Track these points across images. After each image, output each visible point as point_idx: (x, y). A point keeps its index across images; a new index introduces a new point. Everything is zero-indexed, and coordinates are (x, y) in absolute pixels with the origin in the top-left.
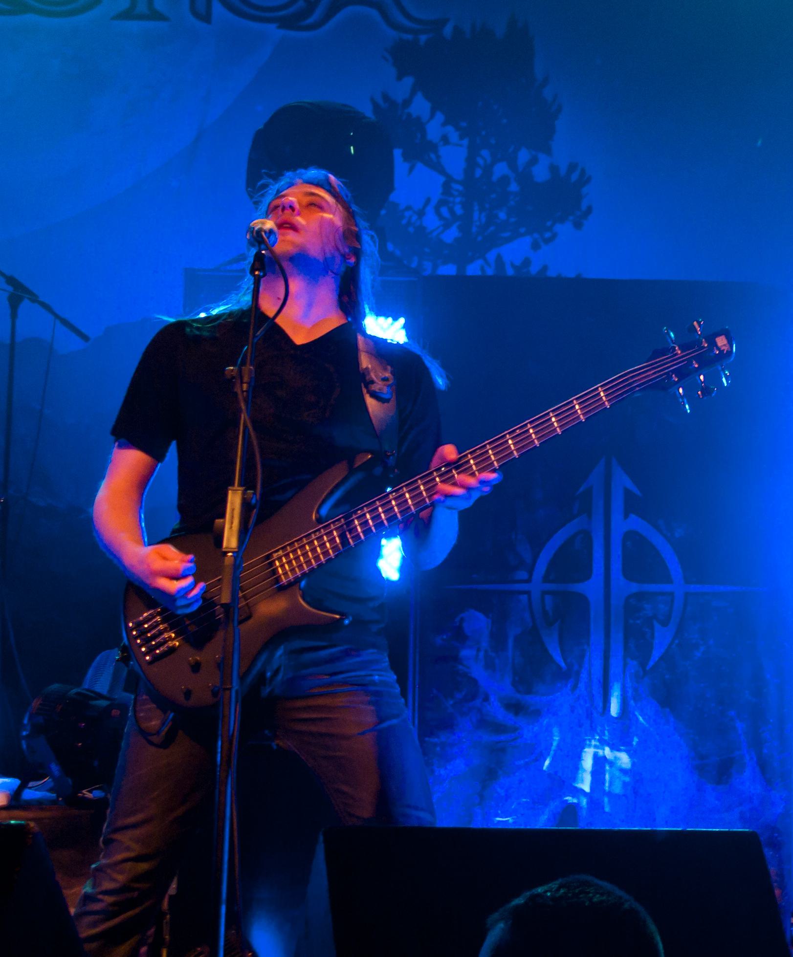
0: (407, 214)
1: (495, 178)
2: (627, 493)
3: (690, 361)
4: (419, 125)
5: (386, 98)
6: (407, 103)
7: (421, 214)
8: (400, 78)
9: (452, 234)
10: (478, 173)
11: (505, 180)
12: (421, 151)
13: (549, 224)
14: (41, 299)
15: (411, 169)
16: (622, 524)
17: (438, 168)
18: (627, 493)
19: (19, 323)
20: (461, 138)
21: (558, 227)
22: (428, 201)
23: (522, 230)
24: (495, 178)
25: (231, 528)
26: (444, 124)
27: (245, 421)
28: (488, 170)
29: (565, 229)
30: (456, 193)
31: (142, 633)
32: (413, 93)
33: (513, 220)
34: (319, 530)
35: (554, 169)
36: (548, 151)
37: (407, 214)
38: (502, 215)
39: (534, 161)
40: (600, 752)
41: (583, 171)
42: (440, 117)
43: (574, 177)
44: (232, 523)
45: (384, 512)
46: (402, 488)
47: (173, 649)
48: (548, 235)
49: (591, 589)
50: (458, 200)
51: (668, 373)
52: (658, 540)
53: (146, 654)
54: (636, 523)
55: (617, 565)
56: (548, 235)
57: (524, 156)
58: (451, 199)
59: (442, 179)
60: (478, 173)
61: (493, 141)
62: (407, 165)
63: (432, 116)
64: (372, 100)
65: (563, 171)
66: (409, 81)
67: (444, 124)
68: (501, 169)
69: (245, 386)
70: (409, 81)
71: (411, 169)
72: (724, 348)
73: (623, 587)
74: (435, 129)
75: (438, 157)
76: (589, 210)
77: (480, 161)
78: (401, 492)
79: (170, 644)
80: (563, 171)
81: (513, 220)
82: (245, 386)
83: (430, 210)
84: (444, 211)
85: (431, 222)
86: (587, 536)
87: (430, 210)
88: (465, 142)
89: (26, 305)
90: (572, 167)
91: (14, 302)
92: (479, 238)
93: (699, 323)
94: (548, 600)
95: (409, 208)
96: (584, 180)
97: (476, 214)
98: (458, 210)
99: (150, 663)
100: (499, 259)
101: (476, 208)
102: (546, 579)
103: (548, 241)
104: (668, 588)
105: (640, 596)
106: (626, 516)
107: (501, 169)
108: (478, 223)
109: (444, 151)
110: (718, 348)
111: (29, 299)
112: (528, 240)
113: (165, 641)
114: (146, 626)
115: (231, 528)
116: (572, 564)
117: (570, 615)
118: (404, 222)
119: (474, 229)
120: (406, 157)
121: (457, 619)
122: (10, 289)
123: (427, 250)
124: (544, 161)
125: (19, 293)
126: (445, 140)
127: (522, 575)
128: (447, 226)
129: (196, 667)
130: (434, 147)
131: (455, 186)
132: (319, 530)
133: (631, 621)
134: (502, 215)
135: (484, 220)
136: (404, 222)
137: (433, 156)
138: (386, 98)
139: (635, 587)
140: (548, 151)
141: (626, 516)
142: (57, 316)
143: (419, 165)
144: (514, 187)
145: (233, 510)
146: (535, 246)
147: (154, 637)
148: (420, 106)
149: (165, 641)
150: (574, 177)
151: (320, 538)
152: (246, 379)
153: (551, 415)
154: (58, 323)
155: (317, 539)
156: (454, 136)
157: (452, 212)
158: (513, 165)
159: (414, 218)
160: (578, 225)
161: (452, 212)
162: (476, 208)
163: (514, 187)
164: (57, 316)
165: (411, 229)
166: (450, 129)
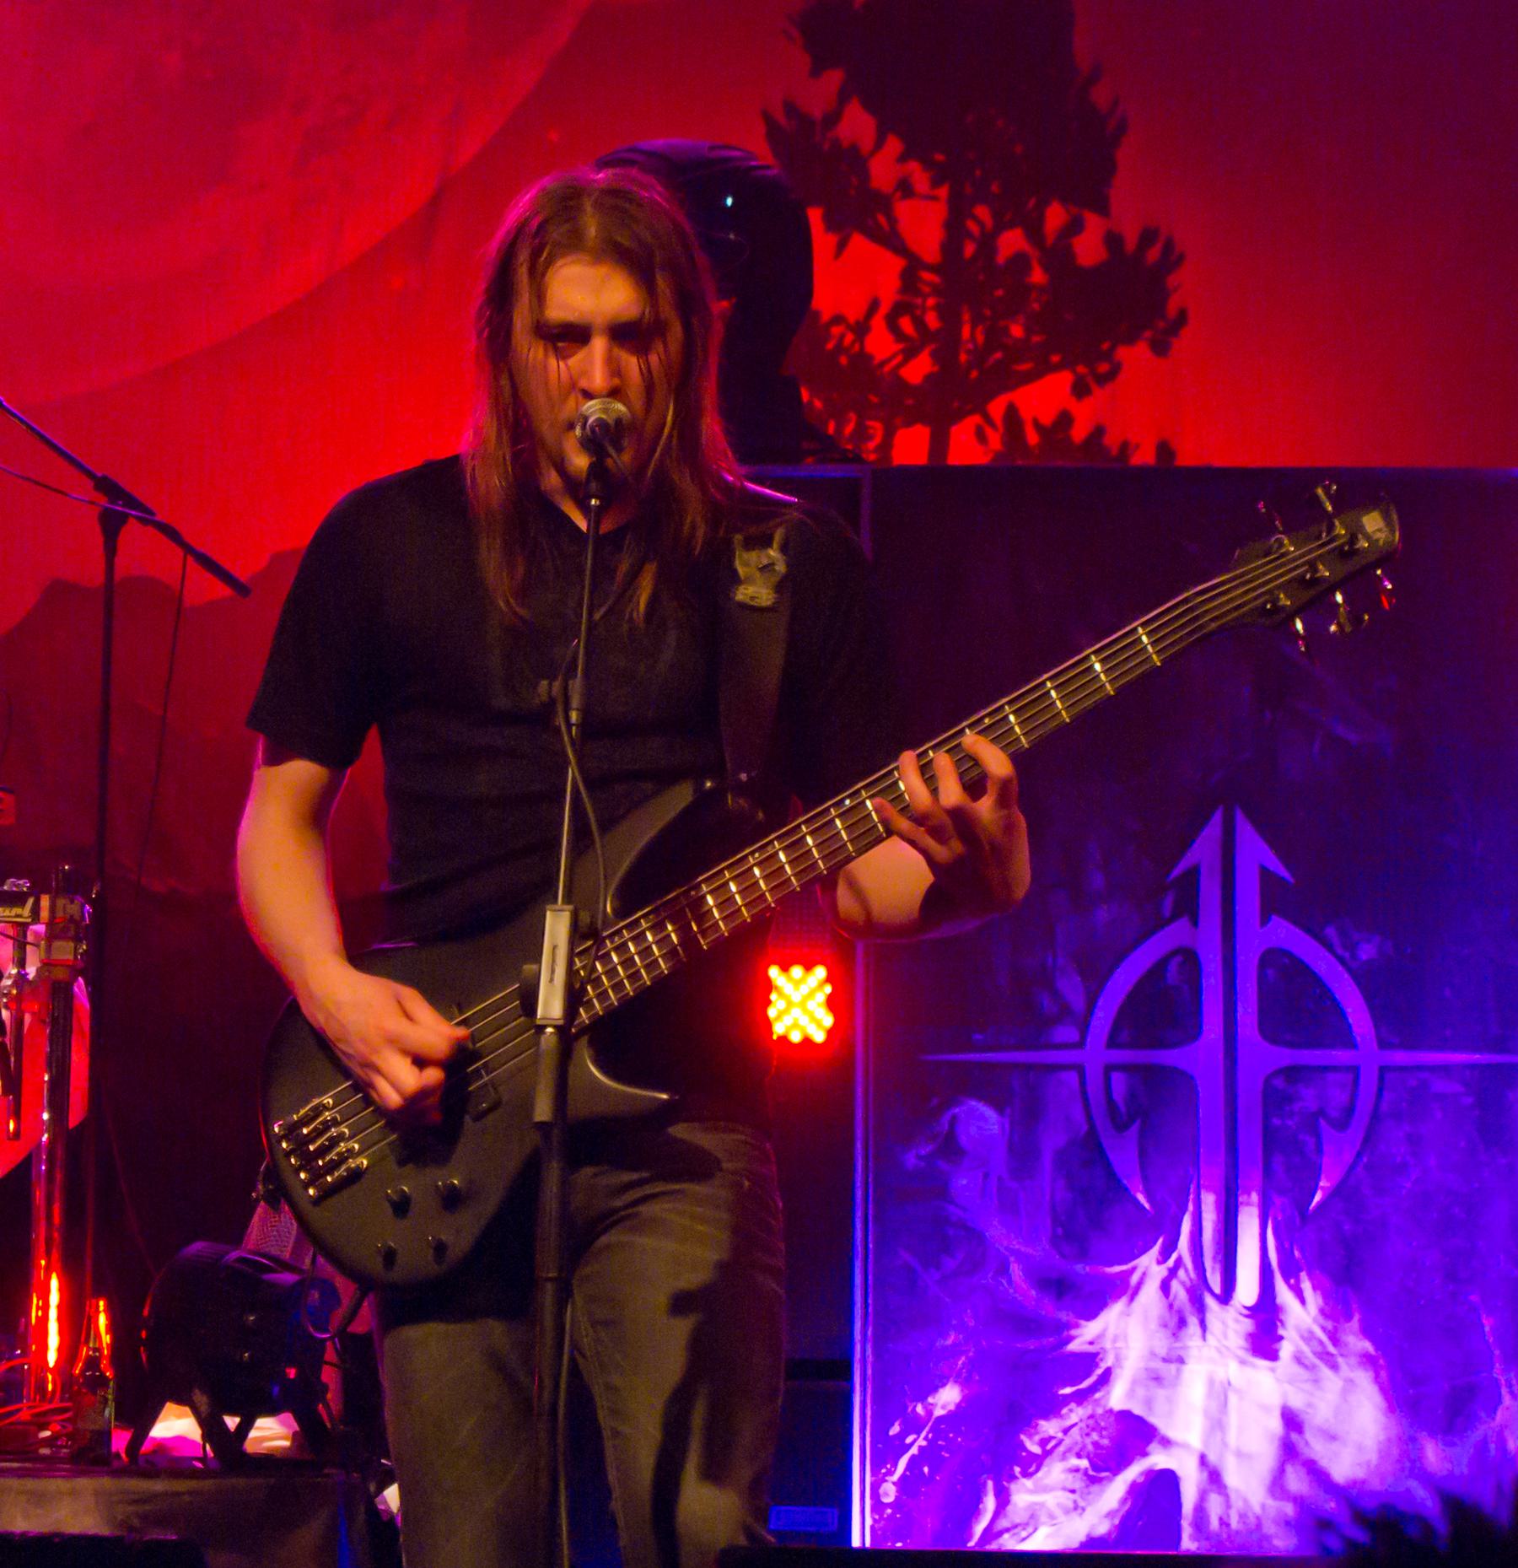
0: (836, 330)
1: (1001, 259)
2: (1264, 870)
3: (1312, 566)
4: (856, 160)
5: (790, 109)
6: (833, 119)
7: (861, 329)
8: (816, 71)
9: (919, 369)
10: (969, 249)
11: (1020, 263)
12: (863, 213)
13: (1105, 346)
14: (158, 518)
15: (841, 246)
16: (1266, 935)
17: (892, 241)
18: (1264, 870)
19: (119, 560)
20: (936, 183)
21: (1123, 353)
22: (874, 306)
23: (1055, 359)
24: (1001, 259)
25: (551, 980)
26: (903, 158)
27: (574, 778)
28: (987, 244)
29: (1135, 356)
30: (927, 290)
31: (301, 1144)
32: (843, 97)
33: (1036, 339)
34: (619, 932)
35: (1113, 241)
36: (1103, 209)
37: (836, 330)
38: (1017, 331)
39: (1074, 227)
40: (1221, 1374)
41: (1169, 246)
42: (893, 145)
43: (1153, 254)
44: (553, 972)
45: (739, 892)
46: (771, 842)
47: (356, 1175)
48: (1104, 368)
49: (1199, 1058)
50: (931, 302)
51: (1270, 592)
52: (1322, 963)
53: (306, 1185)
54: (1283, 933)
55: (1247, 1012)
56: (1104, 368)
57: (1055, 216)
58: (919, 301)
59: (897, 264)
60: (969, 249)
61: (995, 188)
62: (832, 239)
63: (879, 144)
64: (768, 119)
65: (1131, 244)
66: (834, 78)
67: (903, 158)
68: (1012, 241)
69: (574, 716)
70: (834, 78)
71: (841, 246)
72: (1378, 535)
73: (1262, 1057)
74: (884, 169)
75: (893, 221)
76: (1182, 318)
77: (972, 226)
78: (770, 851)
79: (352, 1163)
80: (1131, 244)
81: (1036, 339)
82: (574, 716)
83: (878, 322)
84: (906, 324)
85: (880, 344)
86: (1190, 959)
87: (878, 322)
88: (943, 192)
89: (133, 534)
90: (1148, 237)
91: (111, 525)
92: (974, 374)
93: (1327, 490)
94: (1119, 1081)
95: (838, 319)
96: (1171, 260)
97: (966, 332)
98: (932, 321)
99: (316, 1201)
100: (1012, 415)
101: (966, 317)
102: (1113, 1043)
103: (1103, 380)
104: (1339, 1056)
105: (1293, 1073)
106: (1265, 920)
107: (1012, 241)
108: (971, 346)
109: (904, 210)
110: (1368, 537)
111: (139, 519)
112: (1065, 379)
113: (343, 1159)
114: (305, 1131)
115: (551, 980)
116: (1162, 1011)
117: (1153, 1103)
118: (830, 346)
119: (963, 357)
120: (831, 224)
121: (945, 1121)
122: (103, 501)
123: (875, 399)
124: (1094, 225)
125: (118, 508)
126: (906, 188)
127: (1066, 1033)
128: (910, 353)
129: (401, 1207)
130: (883, 203)
131: (927, 276)
132: (619, 932)
133: (1276, 1121)
134: (1017, 331)
135: (980, 338)
136: (830, 346)
137: (882, 219)
138: (790, 109)
139: (1287, 1056)
140: (1103, 209)
141: (1265, 920)
142: (188, 549)
143: (858, 241)
144: (1038, 276)
145: (555, 948)
146: (1080, 390)
147: (322, 1151)
148: (857, 125)
149: (343, 1159)
150: (1153, 254)
151: (621, 949)
152: (575, 702)
153: (1049, 684)
154: (190, 559)
155: (616, 949)
156: (920, 179)
157: (919, 323)
158: (1034, 231)
159: (849, 338)
160: (1160, 348)
161: (919, 323)
162: (966, 317)
163: (1038, 276)
164: (188, 549)
165: (844, 360)
166: (914, 168)
